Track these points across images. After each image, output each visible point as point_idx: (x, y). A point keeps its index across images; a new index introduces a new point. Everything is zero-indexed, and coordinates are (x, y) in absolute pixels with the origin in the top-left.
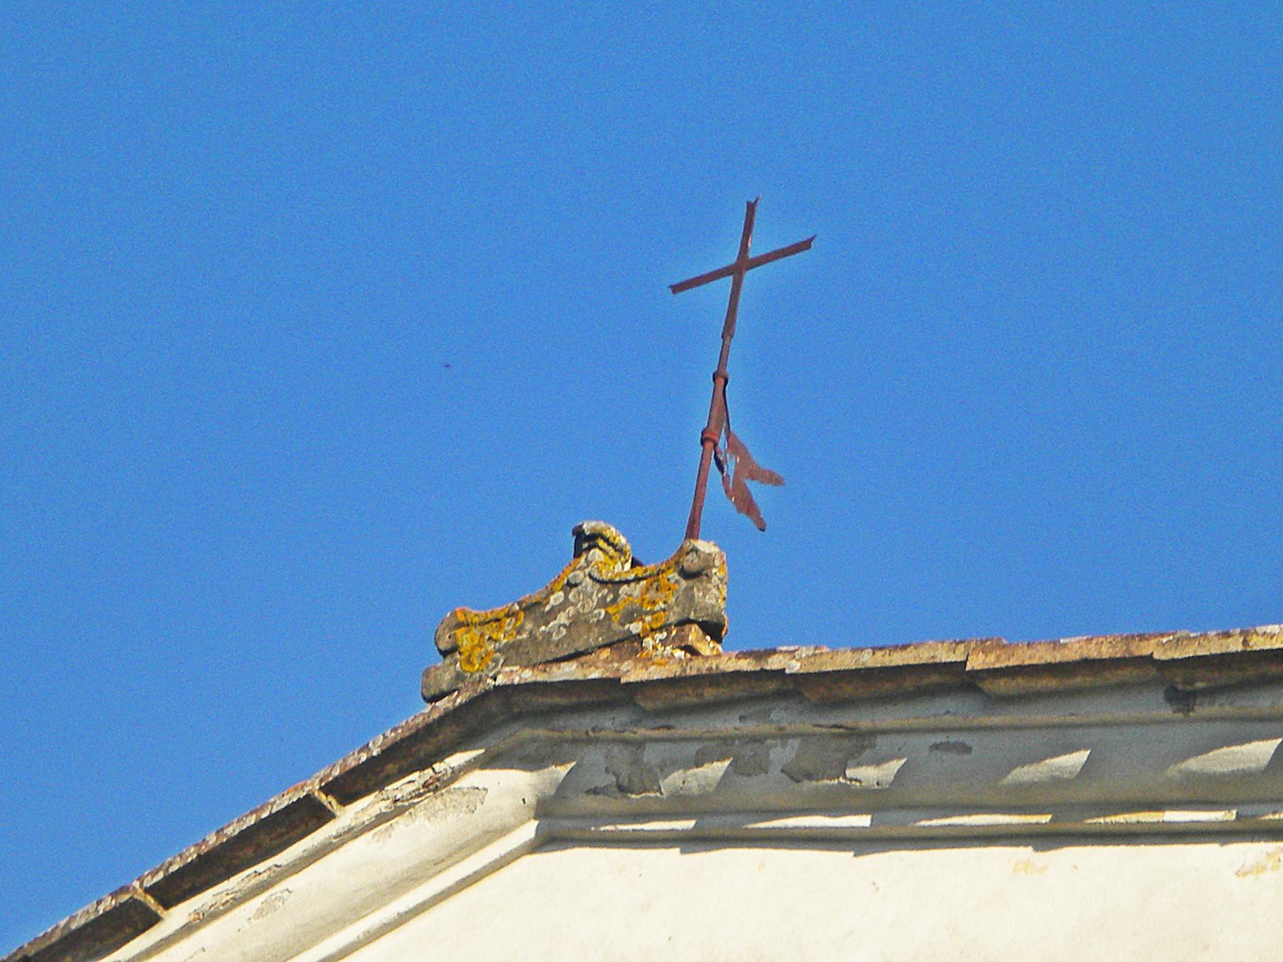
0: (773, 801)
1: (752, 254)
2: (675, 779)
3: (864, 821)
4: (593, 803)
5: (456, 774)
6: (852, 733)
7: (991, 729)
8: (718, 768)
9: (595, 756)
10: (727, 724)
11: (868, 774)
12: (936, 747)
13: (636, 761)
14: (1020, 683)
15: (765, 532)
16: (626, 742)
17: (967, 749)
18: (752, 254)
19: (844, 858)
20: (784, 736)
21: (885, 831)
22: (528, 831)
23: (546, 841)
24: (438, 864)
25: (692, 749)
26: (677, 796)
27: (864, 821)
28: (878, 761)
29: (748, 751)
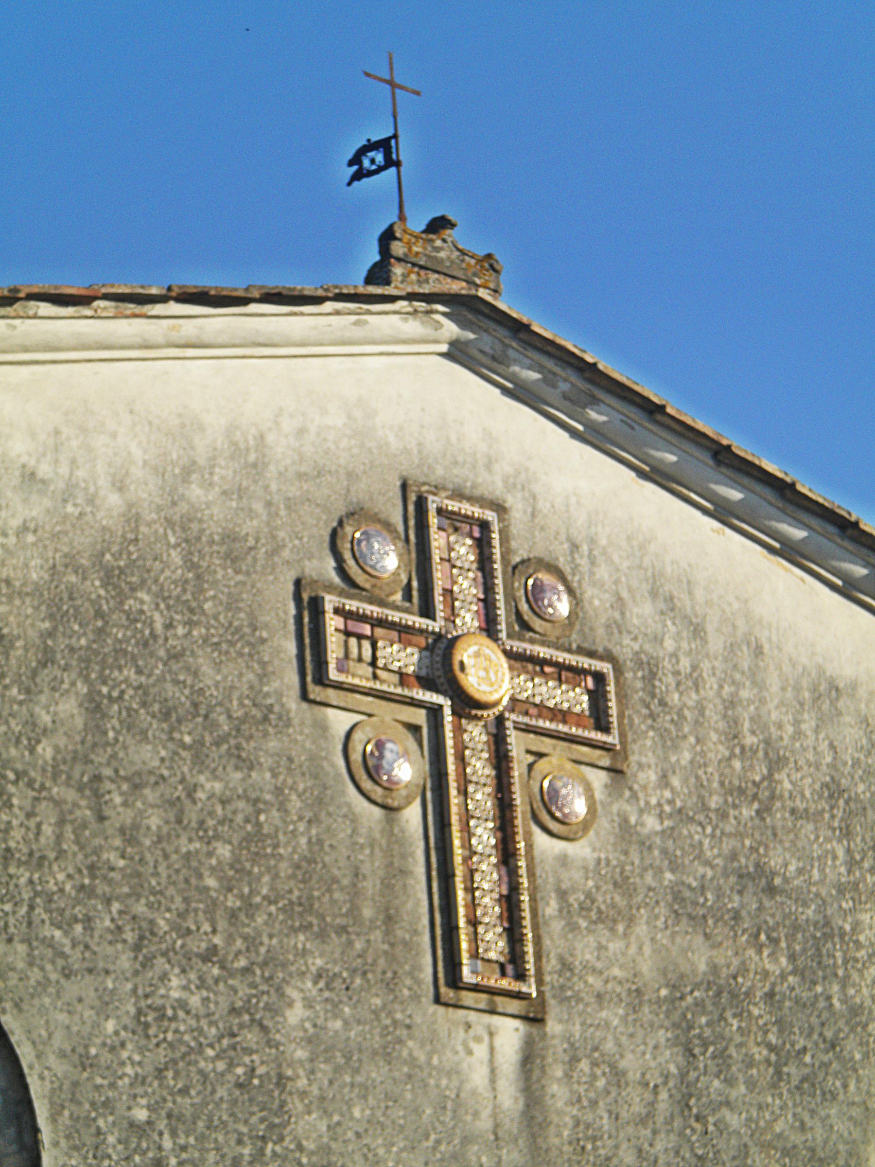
0: (555, 402)
1: (397, 91)
2: (516, 369)
3: (580, 428)
4: (479, 356)
5: (437, 312)
6: (593, 396)
7: (646, 428)
8: (535, 376)
9: (487, 338)
10: (550, 364)
11: (593, 415)
12: (622, 421)
13: (504, 352)
14: (673, 425)
15: (490, 251)
16: (503, 342)
17: (632, 428)
18: (397, 91)
19: (565, 435)
20: (565, 380)
21: (587, 436)
22: (444, 348)
23: (446, 355)
24: (414, 341)
25: (528, 362)
26: (514, 374)
27: (580, 428)
28: (599, 413)
29: (550, 376)
